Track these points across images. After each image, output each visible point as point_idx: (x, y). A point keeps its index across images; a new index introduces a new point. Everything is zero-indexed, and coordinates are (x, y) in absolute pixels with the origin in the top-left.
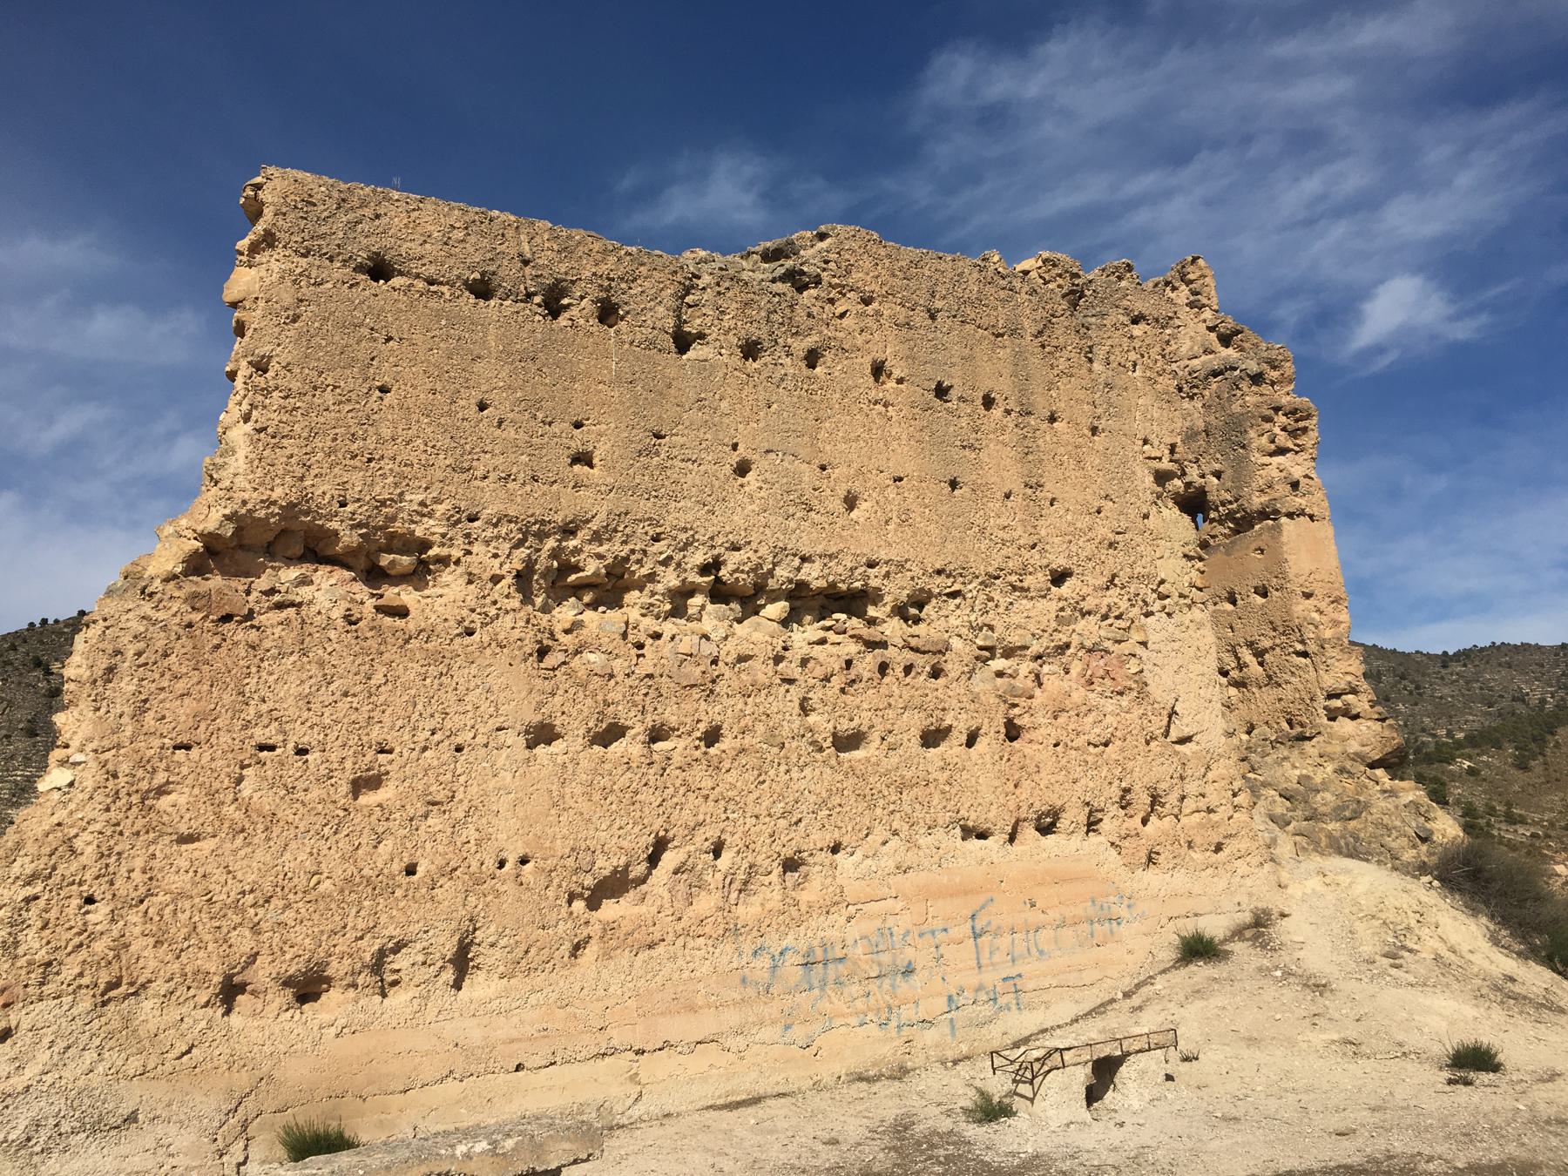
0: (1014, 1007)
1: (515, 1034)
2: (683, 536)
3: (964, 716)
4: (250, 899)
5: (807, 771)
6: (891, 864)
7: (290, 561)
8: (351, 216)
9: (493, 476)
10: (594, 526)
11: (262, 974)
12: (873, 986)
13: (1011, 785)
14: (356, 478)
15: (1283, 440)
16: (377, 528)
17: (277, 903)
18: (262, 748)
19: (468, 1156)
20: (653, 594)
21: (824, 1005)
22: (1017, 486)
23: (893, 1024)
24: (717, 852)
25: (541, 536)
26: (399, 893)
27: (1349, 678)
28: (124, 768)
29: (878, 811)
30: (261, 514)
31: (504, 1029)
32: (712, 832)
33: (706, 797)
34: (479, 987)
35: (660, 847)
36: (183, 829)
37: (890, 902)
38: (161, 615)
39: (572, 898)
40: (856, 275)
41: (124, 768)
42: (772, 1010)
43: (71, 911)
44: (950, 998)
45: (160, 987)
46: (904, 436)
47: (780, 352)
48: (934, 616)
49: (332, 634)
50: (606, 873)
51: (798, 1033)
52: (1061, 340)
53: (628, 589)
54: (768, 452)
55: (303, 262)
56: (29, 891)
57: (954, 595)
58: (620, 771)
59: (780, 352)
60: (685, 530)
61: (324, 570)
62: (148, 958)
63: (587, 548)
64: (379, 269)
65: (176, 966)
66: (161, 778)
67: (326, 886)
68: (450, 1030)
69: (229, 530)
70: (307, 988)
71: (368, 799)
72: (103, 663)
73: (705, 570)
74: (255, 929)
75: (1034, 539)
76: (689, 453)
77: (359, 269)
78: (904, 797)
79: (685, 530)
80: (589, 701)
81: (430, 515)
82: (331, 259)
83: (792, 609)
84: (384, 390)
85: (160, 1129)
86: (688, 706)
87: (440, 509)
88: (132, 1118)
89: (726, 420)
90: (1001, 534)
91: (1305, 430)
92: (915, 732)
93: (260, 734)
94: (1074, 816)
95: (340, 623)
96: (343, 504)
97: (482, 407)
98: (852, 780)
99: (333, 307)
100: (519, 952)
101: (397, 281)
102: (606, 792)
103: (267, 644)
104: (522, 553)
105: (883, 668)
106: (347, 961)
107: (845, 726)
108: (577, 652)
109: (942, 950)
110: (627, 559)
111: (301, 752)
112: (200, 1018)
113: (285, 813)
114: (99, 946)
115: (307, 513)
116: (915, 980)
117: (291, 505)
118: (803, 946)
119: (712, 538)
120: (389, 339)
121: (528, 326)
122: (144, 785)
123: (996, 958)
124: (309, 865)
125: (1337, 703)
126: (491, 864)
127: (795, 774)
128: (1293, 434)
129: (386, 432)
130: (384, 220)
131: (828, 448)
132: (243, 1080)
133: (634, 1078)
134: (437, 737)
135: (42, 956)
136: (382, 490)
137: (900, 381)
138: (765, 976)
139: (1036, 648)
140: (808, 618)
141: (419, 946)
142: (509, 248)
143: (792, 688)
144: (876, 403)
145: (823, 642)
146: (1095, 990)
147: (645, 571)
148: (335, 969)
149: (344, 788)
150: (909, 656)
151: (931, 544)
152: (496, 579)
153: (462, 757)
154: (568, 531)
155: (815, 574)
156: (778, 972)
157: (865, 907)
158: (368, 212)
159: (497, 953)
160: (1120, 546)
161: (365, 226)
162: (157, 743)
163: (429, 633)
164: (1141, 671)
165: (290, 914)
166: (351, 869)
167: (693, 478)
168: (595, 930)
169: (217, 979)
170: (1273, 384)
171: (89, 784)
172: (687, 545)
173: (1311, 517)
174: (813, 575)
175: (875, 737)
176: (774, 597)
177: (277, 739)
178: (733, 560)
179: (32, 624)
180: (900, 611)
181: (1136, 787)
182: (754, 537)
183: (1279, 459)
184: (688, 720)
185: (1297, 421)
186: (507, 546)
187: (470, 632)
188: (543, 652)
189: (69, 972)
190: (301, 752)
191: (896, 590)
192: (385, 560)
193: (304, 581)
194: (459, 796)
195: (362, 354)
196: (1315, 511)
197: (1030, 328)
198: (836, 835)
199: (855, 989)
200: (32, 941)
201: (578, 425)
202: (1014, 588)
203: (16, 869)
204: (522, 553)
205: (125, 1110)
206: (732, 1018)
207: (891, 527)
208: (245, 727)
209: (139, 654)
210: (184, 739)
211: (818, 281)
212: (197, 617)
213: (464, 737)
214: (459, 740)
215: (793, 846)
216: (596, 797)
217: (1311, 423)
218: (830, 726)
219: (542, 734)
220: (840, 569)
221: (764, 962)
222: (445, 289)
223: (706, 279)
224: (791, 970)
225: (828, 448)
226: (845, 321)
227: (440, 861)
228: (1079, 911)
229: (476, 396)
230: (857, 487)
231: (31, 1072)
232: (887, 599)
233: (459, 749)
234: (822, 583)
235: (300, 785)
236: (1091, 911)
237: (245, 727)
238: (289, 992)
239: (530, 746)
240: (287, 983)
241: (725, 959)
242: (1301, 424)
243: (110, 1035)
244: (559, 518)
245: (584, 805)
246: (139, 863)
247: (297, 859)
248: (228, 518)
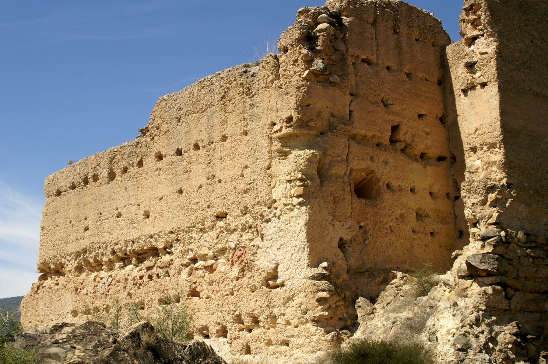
22: (204, 181)
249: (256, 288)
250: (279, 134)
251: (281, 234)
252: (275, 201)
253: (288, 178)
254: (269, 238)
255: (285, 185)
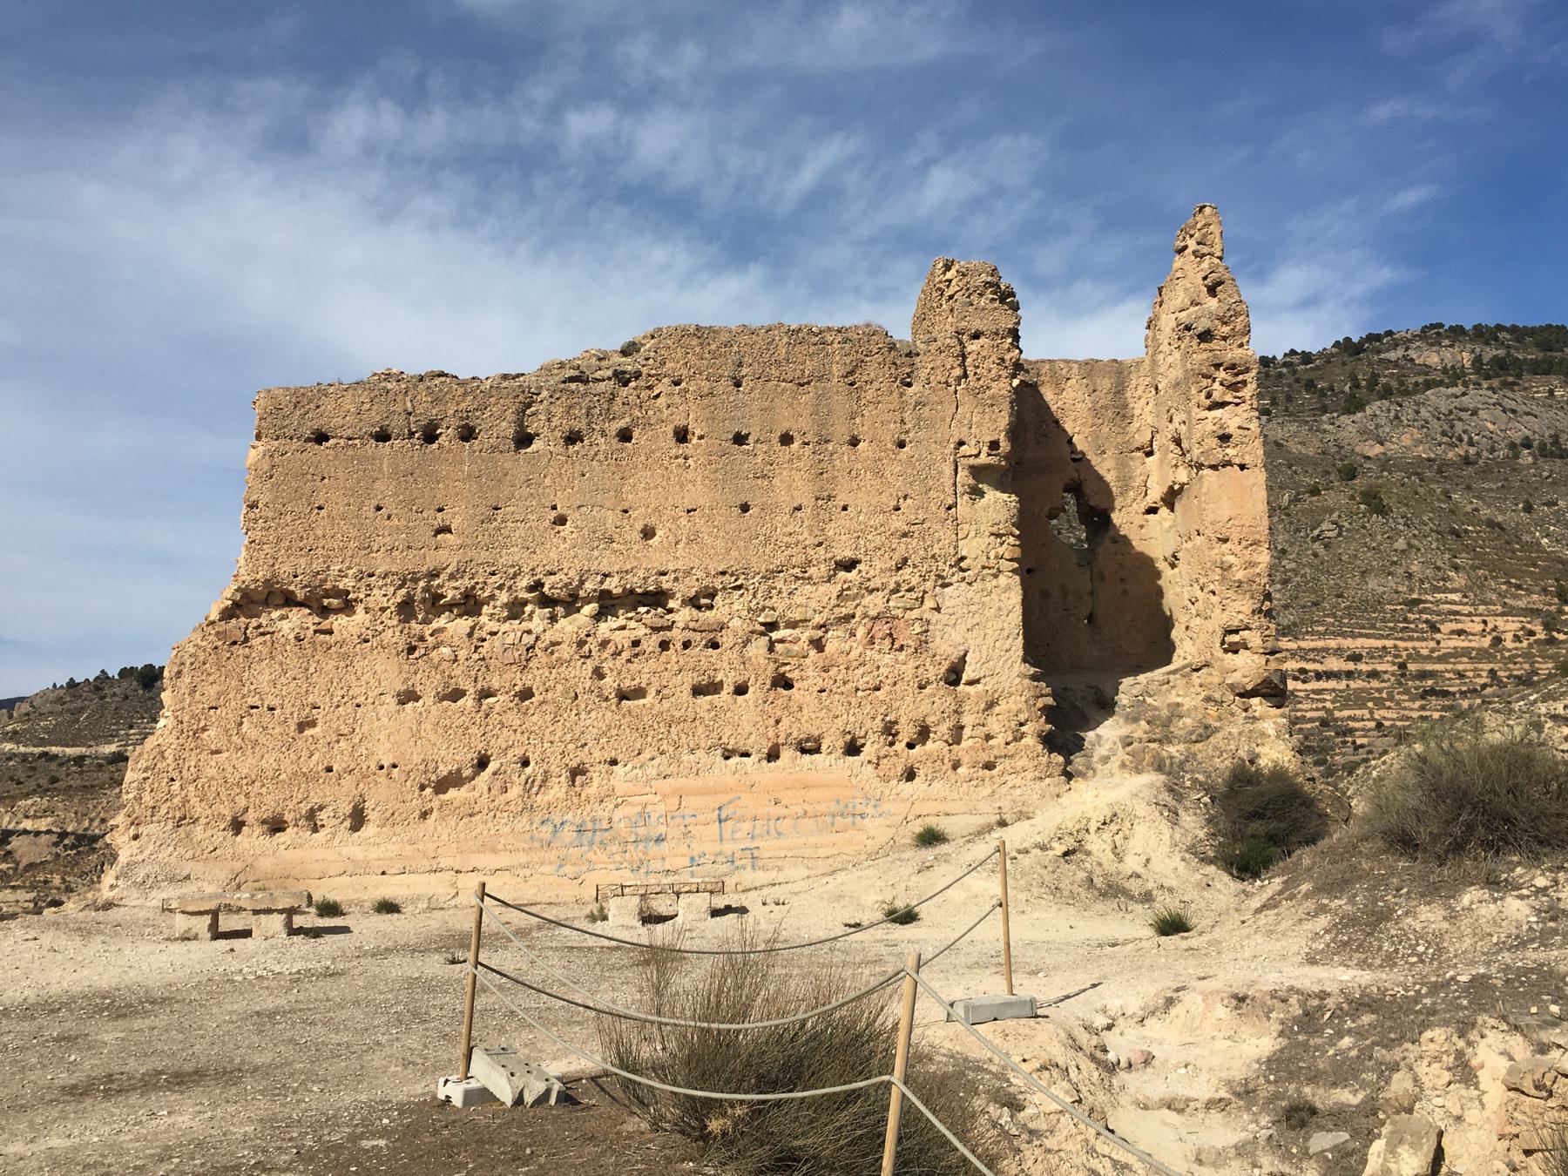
0: (749, 868)
1: (381, 856)
2: (512, 571)
3: (733, 674)
4: (245, 781)
5: (593, 714)
6: (654, 773)
7: (277, 607)
8: (302, 411)
9: (383, 549)
10: (449, 571)
11: (250, 817)
12: (630, 847)
13: (772, 721)
14: (303, 561)
15: (1218, 392)
16: (316, 587)
17: (258, 784)
18: (253, 707)
19: (239, 899)
20: (495, 607)
21: (590, 855)
22: (807, 500)
23: (643, 870)
24: (526, 763)
25: (415, 580)
26: (321, 781)
27: (1241, 616)
28: (186, 719)
29: (649, 739)
30: (253, 587)
31: (376, 853)
32: (519, 751)
33: (515, 731)
34: (368, 831)
35: (482, 763)
36: (213, 747)
37: (650, 796)
38: (204, 643)
39: (422, 788)
40: (669, 365)
41: (186, 719)
42: (553, 855)
43: (164, 784)
44: (692, 859)
45: (203, 821)
46: (699, 478)
47: (597, 435)
48: (721, 603)
49: (288, 648)
50: (445, 773)
51: (569, 870)
52: (872, 374)
53: (483, 604)
54: (579, 507)
55: (276, 443)
56: (145, 775)
57: (739, 587)
58: (457, 715)
59: (597, 435)
60: (513, 566)
61: (295, 610)
62: (198, 808)
63: (447, 584)
64: (321, 437)
65: (209, 812)
66: (202, 723)
67: (283, 776)
68: (346, 851)
69: (238, 596)
70: (276, 826)
71: (308, 732)
72: (175, 669)
73: (531, 589)
74: (247, 795)
75: (820, 539)
76: (517, 517)
77: (308, 440)
78: (673, 729)
79: (513, 566)
80: (439, 676)
81: (346, 576)
82: (291, 438)
83: (601, 607)
84: (320, 508)
85: (200, 884)
86: (507, 676)
87: (351, 572)
88: (188, 877)
89: (547, 490)
90: (786, 539)
91: (1244, 383)
92: (687, 688)
93: (251, 701)
94: (833, 741)
95: (293, 641)
96: (295, 576)
97: (379, 508)
98: (628, 719)
99: (290, 466)
100: (388, 814)
101: (332, 442)
102: (446, 729)
103: (254, 655)
104: (404, 591)
105: (664, 645)
106: (292, 814)
107: (627, 684)
108: (434, 648)
109: (689, 828)
110: (473, 588)
111: (272, 709)
112: (220, 836)
113: (262, 740)
114: (176, 801)
115: (278, 583)
116: (665, 845)
117: (267, 581)
118: (578, 820)
119: (533, 570)
120: (323, 478)
121: (410, 454)
122: (195, 727)
123: (738, 835)
124: (275, 766)
125: (1235, 638)
126: (373, 767)
127: (583, 716)
128: (1234, 387)
129: (320, 533)
130: (322, 408)
131: (630, 497)
132: (238, 866)
133: (454, 885)
134: (346, 699)
135: (151, 804)
136: (316, 566)
137: (701, 437)
138: (548, 836)
139: (818, 619)
140: (621, 611)
141: (331, 808)
142: (398, 408)
143: (588, 661)
144: (677, 457)
145: (623, 628)
146: (830, 861)
147: (486, 594)
148: (288, 817)
149: (293, 727)
150: (689, 635)
151: (716, 554)
152: (383, 610)
153: (360, 710)
154: (434, 575)
155: (613, 585)
156: (558, 834)
157: (630, 799)
158: (312, 406)
159: (375, 813)
160: (916, 535)
161: (310, 415)
162: (201, 706)
163: (343, 643)
164: (927, 631)
165: (264, 789)
166: (296, 768)
167: (521, 530)
168: (436, 804)
169: (229, 818)
170: (1224, 339)
171: (170, 727)
172: (515, 576)
173: (1242, 467)
174: (613, 585)
175: (652, 692)
176: (587, 601)
177: (258, 703)
178: (548, 582)
179: (87, 680)
180: (693, 602)
181: (903, 720)
182: (565, 565)
183: (1218, 413)
184: (507, 685)
185: (1237, 375)
186: (393, 589)
187: (367, 641)
188: (412, 650)
189: (163, 811)
190: (272, 709)
191: (689, 587)
192: (326, 602)
193: (282, 618)
194: (357, 731)
195: (307, 490)
196: (1247, 460)
197: (837, 370)
198: (613, 754)
199: (615, 848)
200: (147, 797)
201: (441, 510)
202: (797, 578)
203: (139, 766)
204: (404, 591)
205: (185, 874)
206: (522, 858)
207: (680, 546)
208: (243, 698)
209: (192, 664)
210: (214, 704)
211: (638, 375)
212: (220, 643)
213: (361, 699)
214: (357, 701)
215: (578, 760)
216: (440, 731)
217: (1249, 377)
218: (615, 685)
219: (408, 697)
220: (636, 579)
221: (548, 828)
222: (357, 441)
223: (545, 394)
224: (568, 834)
225: (630, 497)
226: (659, 400)
227: (344, 765)
228: (823, 808)
229: (375, 503)
230: (653, 521)
231: (146, 853)
232: (678, 595)
233: (358, 706)
234: (620, 590)
235: (270, 726)
236: (834, 808)
237: (243, 698)
238: (266, 827)
239: (402, 703)
240: (264, 822)
241: (520, 825)
242: (1240, 378)
243: (180, 840)
244: (424, 569)
245: (432, 736)
246: (193, 763)
247: (269, 762)
248: (237, 590)
249: (928, 683)
250: (972, 461)
251: (973, 608)
252: (963, 559)
253: (995, 530)
254: (951, 611)
255: (987, 540)
